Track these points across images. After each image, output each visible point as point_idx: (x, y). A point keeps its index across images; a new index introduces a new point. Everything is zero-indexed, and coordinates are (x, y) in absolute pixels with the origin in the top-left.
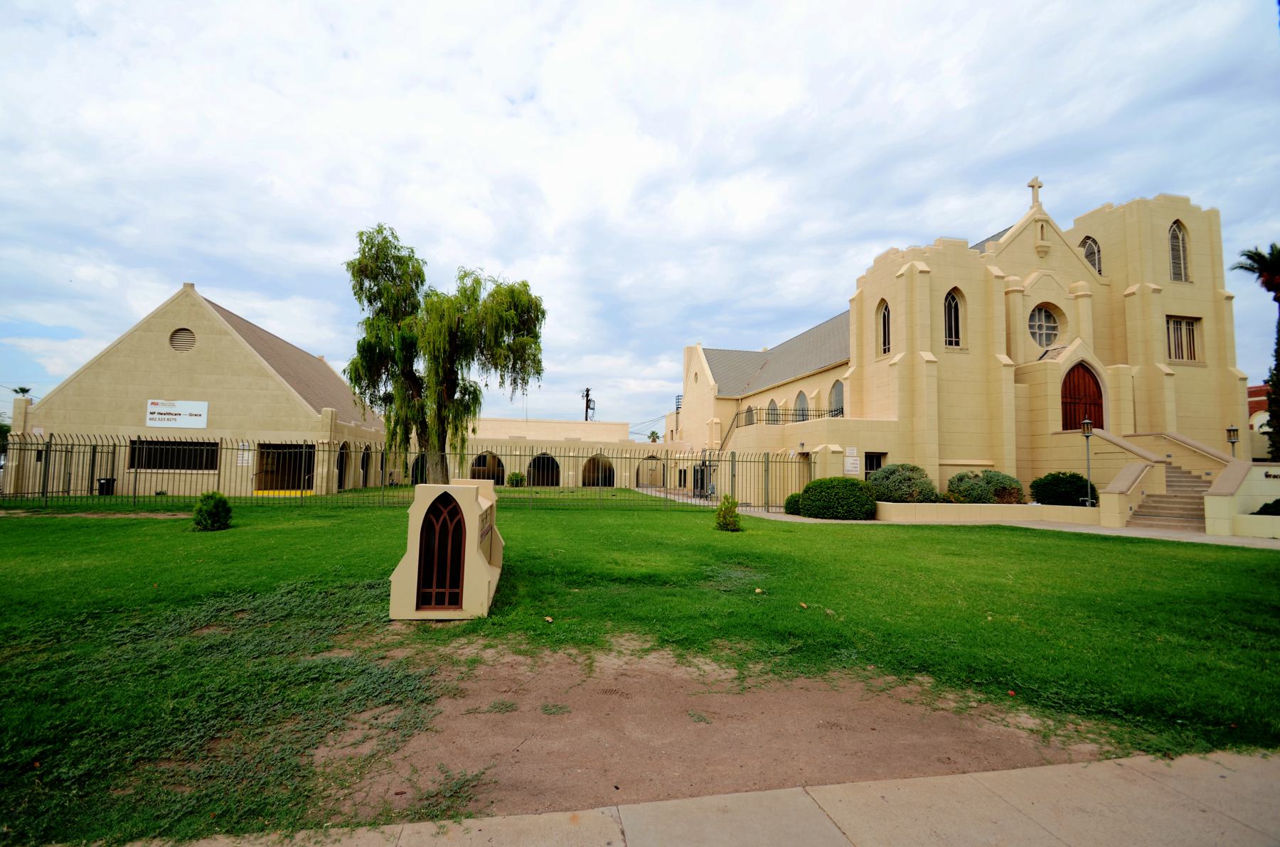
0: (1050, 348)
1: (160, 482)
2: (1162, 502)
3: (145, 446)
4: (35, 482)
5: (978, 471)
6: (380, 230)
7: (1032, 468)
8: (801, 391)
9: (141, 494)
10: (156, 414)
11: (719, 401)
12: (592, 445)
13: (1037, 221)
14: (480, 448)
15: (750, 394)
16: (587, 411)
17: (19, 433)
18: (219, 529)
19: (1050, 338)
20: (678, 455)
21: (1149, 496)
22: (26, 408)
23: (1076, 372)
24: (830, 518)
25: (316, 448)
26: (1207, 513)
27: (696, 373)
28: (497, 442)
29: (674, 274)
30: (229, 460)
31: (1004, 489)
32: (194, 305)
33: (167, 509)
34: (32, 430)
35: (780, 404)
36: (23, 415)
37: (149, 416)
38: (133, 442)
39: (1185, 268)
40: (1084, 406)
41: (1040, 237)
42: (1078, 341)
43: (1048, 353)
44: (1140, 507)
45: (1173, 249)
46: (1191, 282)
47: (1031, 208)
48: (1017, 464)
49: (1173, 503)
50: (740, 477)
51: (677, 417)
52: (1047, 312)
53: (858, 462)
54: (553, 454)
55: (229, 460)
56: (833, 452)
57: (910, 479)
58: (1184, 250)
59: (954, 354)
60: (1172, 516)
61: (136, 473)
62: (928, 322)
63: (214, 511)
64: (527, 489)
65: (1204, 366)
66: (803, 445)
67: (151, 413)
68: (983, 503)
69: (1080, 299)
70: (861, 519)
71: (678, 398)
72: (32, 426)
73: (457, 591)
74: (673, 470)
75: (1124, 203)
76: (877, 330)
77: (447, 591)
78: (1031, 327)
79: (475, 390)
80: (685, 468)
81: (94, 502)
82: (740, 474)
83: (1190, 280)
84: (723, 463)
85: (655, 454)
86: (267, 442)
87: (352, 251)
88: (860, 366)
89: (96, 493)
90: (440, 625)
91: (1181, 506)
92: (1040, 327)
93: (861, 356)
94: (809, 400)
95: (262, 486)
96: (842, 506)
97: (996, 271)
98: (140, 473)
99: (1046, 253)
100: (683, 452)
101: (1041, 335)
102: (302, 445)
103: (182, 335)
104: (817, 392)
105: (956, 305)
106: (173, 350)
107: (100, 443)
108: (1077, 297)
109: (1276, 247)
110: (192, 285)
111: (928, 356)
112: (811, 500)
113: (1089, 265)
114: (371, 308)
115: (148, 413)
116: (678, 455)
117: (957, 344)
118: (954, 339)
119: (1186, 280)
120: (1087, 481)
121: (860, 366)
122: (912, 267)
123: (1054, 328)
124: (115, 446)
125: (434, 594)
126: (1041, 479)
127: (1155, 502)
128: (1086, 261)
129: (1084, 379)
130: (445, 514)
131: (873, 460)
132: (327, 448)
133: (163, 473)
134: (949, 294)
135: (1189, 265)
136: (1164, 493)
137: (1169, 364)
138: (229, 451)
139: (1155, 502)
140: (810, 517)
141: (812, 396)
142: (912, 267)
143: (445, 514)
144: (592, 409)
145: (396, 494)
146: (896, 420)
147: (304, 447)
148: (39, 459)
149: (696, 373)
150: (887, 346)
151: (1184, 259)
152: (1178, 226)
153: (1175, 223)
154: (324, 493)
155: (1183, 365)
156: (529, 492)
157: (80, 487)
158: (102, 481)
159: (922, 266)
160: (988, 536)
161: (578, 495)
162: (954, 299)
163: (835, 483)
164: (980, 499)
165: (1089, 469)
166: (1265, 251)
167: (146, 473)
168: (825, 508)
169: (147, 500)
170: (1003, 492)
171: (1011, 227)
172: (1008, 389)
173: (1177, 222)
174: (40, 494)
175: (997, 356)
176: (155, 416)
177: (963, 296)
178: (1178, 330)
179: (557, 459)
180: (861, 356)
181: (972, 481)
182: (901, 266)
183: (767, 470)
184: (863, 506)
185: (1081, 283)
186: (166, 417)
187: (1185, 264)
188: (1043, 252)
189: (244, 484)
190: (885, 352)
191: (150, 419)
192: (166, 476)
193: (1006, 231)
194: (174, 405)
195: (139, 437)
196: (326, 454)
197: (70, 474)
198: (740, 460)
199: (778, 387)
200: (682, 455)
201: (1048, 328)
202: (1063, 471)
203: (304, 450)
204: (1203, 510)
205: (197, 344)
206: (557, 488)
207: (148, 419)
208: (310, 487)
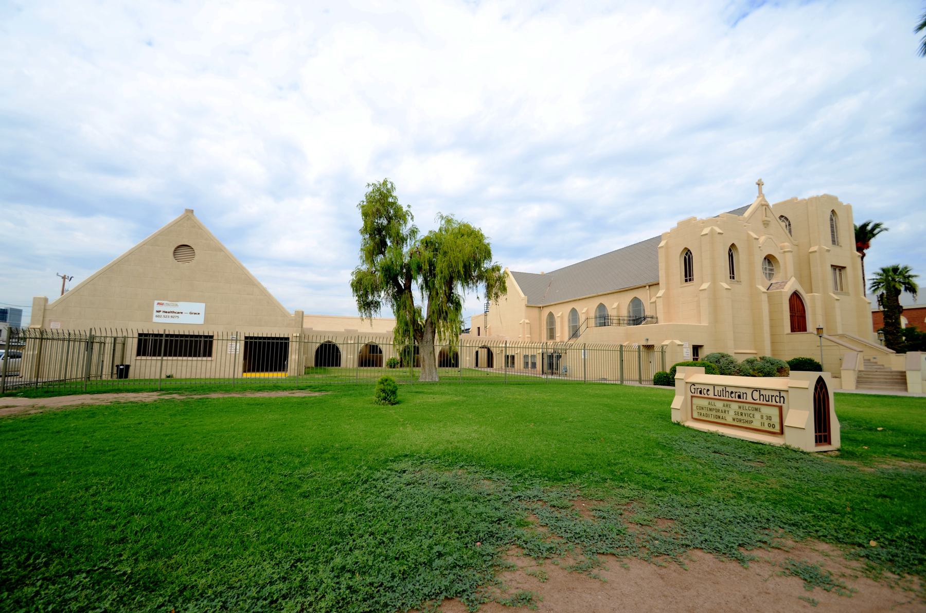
0: (773, 281)
3: (151, 338)
6: (385, 183)
10: (161, 313)
11: (530, 309)
14: (367, 339)
15: (552, 304)
19: (770, 276)
25: (215, 338)
28: (337, 334)
31: (782, 368)
33: (177, 390)
34: (50, 325)
36: (43, 311)
37: (155, 314)
38: (140, 335)
40: (796, 318)
47: (758, 197)
52: (769, 260)
54: (377, 343)
58: (836, 228)
61: (162, 360)
65: (847, 294)
69: (786, 254)
72: (50, 321)
76: (680, 267)
80: (513, 354)
84: (49, 342)
88: (668, 289)
89: (115, 376)
99: (768, 224)
103: (183, 250)
104: (618, 306)
108: (785, 252)
110: (192, 211)
113: (785, 230)
115: (155, 311)
117: (733, 278)
119: (838, 245)
123: (772, 270)
133: (197, 360)
138: (220, 342)
142: (712, 230)
147: (164, 336)
150: (688, 278)
154: (296, 375)
158: (121, 367)
160: (874, 399)
173: (833, 211)
175: (758, 286)
176: (161, 314)
179: (341, 348)
185: (786, 244)
186: (170, 314)
190: (686, 281)
191: (156, 316)
192: (199, 363)
194: (177, 305)
197: (103, 361)
202: (802, 357)
203: (164, 338)
205: (196, 258)
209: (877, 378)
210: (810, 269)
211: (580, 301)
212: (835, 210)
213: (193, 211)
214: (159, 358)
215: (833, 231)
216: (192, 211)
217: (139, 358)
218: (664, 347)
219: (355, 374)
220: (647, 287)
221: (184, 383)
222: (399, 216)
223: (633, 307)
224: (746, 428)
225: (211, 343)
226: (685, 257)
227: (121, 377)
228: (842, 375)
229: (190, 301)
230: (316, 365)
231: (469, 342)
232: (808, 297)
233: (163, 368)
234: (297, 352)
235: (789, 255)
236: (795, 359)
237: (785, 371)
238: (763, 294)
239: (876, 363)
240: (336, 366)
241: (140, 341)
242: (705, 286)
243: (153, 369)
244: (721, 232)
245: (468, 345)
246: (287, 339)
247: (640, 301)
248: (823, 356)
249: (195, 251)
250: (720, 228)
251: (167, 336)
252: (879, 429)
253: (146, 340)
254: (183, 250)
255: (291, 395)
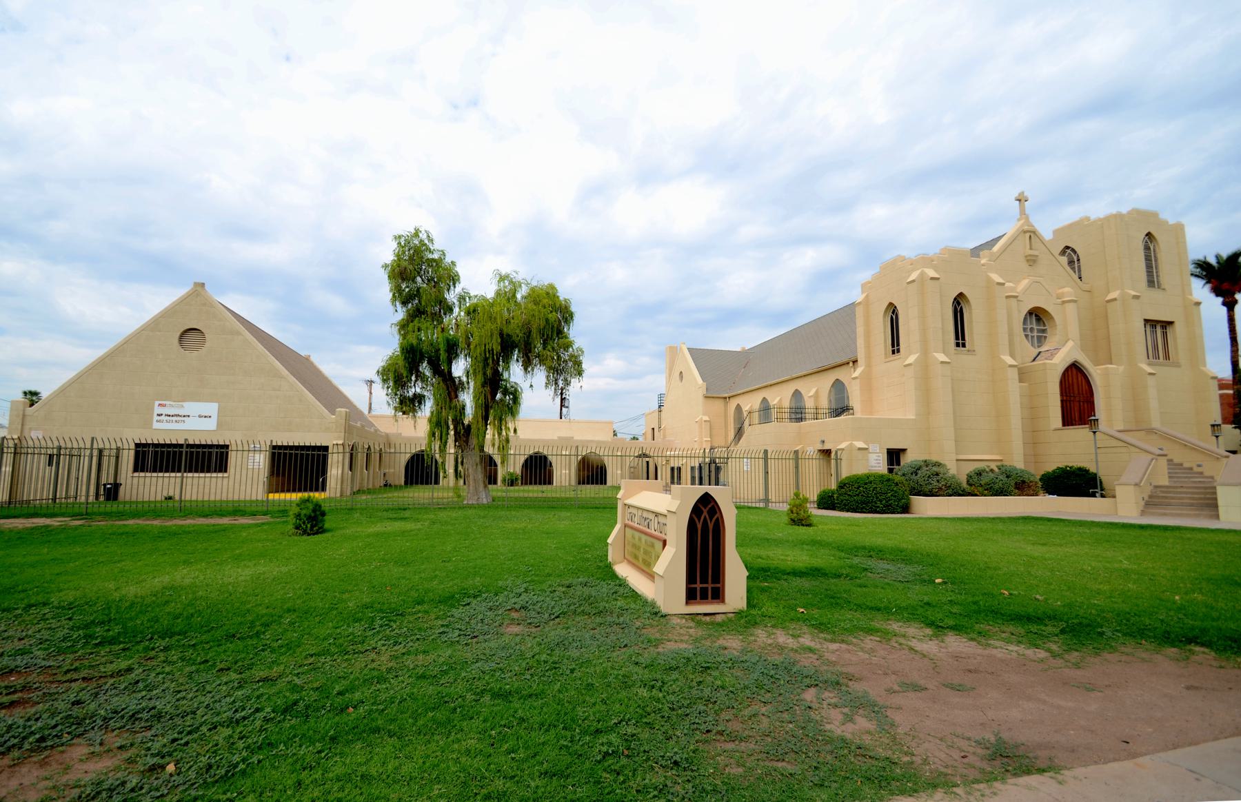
0: (1043, 349)
1: (166, 487)
2: (1170, 492)
3: (151, 449)
4: (30, 487)
5: (993, 466)
6: (417, 233)
7: (1036, 462)
8: (797, 390)
9: (188, 498)
11: (711, 400)
12: (586, 443)
13: (1025, 232)
14: (413, 447)
15: (739, 392)
16: (561, 410)
17: (15, 437)
18: (317, 533)
19: (1041, 340)
20: (668, 453)
21: (1156, 487)
22: (24, 411)
23: (1070, 373)
24: (869, 513)
25: (330, 451)
26: (1220, 502)
27: (681, 372)
28: (547, 443)
29: (618, 275)
30: (239, 463)
31: (1024, 482)
32: (204, 305)
34: (30, 433)
35: (774, 401)
36: (21, 417)
37: (155, 418)
38: (137, 445)
39: (1157, 276)
40: (1077, 404)
41: (1028, 247)
42: (1070, 344)
43: (1041, 354)
44: (1150, 497)
45: (1146, 259)
46: (1164, 289)
48: (1025, 459)
49: (1181, 493)
50: (773, 474)
51: (660, 416)
52: (1037, 315)
53: (881, 458)
55: (239, 463)
56: (859, 449)
57: (937, 474)
58: (1156, 260)
59: (962, 357)
60: (1182, 504)
61: (183, 477)
62: (940, 326)
63: (313, 515)
64: (522, 488)
65: (1178, 365)
66: (823, 442)
67: (159, 415)
68: (1004, 495)
69: (1067, 305)
70: (898, 513)
71: (661, 396)
72: (30, 429)
73: (718, 585)
74: (664, 467)
75: (1102, 217)
76: (885, 332)
77: (710, 586)
78: (1025, 330)
79: (516, 390)
80: (680, 465)
81: (126, 508)
82: (773, 471)
83: (1163, 287)
85: (648, 452)
86: (318, 444)
87: (387, 253)
88: (869, 365)
89: (102, 498)
90: (708, 618)
91: (1189, 496)
92: (1032, 329)
93: (868, 357)
94: (806, 398)
95: (272, 489)
96: (881, 501)
97: (996, 278)
98: (187, 477)
99: (1034, 261)
100: (678, 450)
101: (1032, 337)
102: (182, 445)
103: (192, 335)
104: (816, 392)
105: (961, 309)
106: (182, 350)
107: (107, 446)
108: (1064, 302)
109: (1220, 256)
110: (203, 284)
111: (942, 357)
112: (849, 495)
113: (1071, 272)
114: (404, 309)
116: (668, 453)
117: (964, 345)
118: (960, 341)
119: (1159, 287)
120: (1096, 474)
121: (869, 365)
122: (922, 274)
123: (1044, 331)
124: (118, 449)
125: (698, 589)
126: (1048, 473)
127: (1163, 492)
128: (1068, 269)
129: (1077, 379)
130: (705, 513)
131: (894, 456)
132: (341, 449)
133: (199, 477)
134: (955, 299)
135: (1161, 274)
136: (1167, 483)
137: (1149, 365)
139: (1163, 492)
140: (848, 511)
141: (810, 394)
142: (922, 274)
143: (705, 513)
144: (567, 407)
145: (406, 495)
146: (914, 417)
147: (185, 446)
148: (50, 464)
149: (681, 372)
150: (896, 348)
151: (1156, 268)
152: (1149, 238)
153: (1147, 235)
154: (338, 495)
155: (1160, 365)
156: (537, 491)
157: (85, 493)
158: (109, 486)
159: (932, 273)
161: (572, 494)
162: (959, 303)
163: (872, 479)
164: (1002, 492)
165: (1097, 462)
166: (1212, 261)
167: (145, 477)
168: (863, 503)
169: (200, 505)
170: (1020, 486)
171: (1000, 237)
172: (1014, 390)
173: (1149, 235)
174: (50, 501)
175: (1002, 357)
177: (968, 301)
178: (1154, 333)
179: (550, 458)
180: (868, 357)
181: (992, 475)
182: (910, 272)
183: (797, 467)
184: (900, 500)
185: (1067, 290)
186: (174, 418)
187: (1157, 272)
188: (1032, 261)
189: (255, 486)
190: (893, 352)
192: (220, 481)
193: (1000, 237)
195: (186, 440)
196: (341, 456)
198: (734, 456)
199: (771, 385)
200: (672, 453)
201: (1039, 331)
202: (1071, 465)
204: (1216, 499)
205: (208, 344)
206: (549, 486)
207: (155, 421)
208: (324, 489)
209: (1180, 498)
210: (1108, 327)
211: (773, 388)
212: (1152, 232)
213: (204, 284)
214: (179, 475)
215: (1149, 267)
216: (203, 284)
217: (136, 474)
218: (839, 453)
219: (435, 495)
220: (851, 364)
221: (153, 505)
222: (445, 276)
223: (836, 395)
224: (643, 571)
225: (325, 458)
226: (892, 317)
227: (108, 498)
228: (1117, 494)
229: (199, 401)
230: (406, 483)
231: (620, 449)
232: (1099, 371)
233: (180, 484)
234: (567, 467)
235: (1070, 308)
236: (1058, 468)
237: (1029, 487)
238: (1149, 377)
239: (1202, 473)
240: (601, 484)
241: (137, 453)
242: (911, 359)
243: (153, 489)
244: (936, 275)
245: (619, 454)
246: (326, 448)
247: (843, 384)
248: (1100, 464)
249: (206, 336)
250: (1001, 276)
251: (189, 446)
252: (937, 581)
253: (144, 452)
254: (189, 335)
255: (233, 522)
